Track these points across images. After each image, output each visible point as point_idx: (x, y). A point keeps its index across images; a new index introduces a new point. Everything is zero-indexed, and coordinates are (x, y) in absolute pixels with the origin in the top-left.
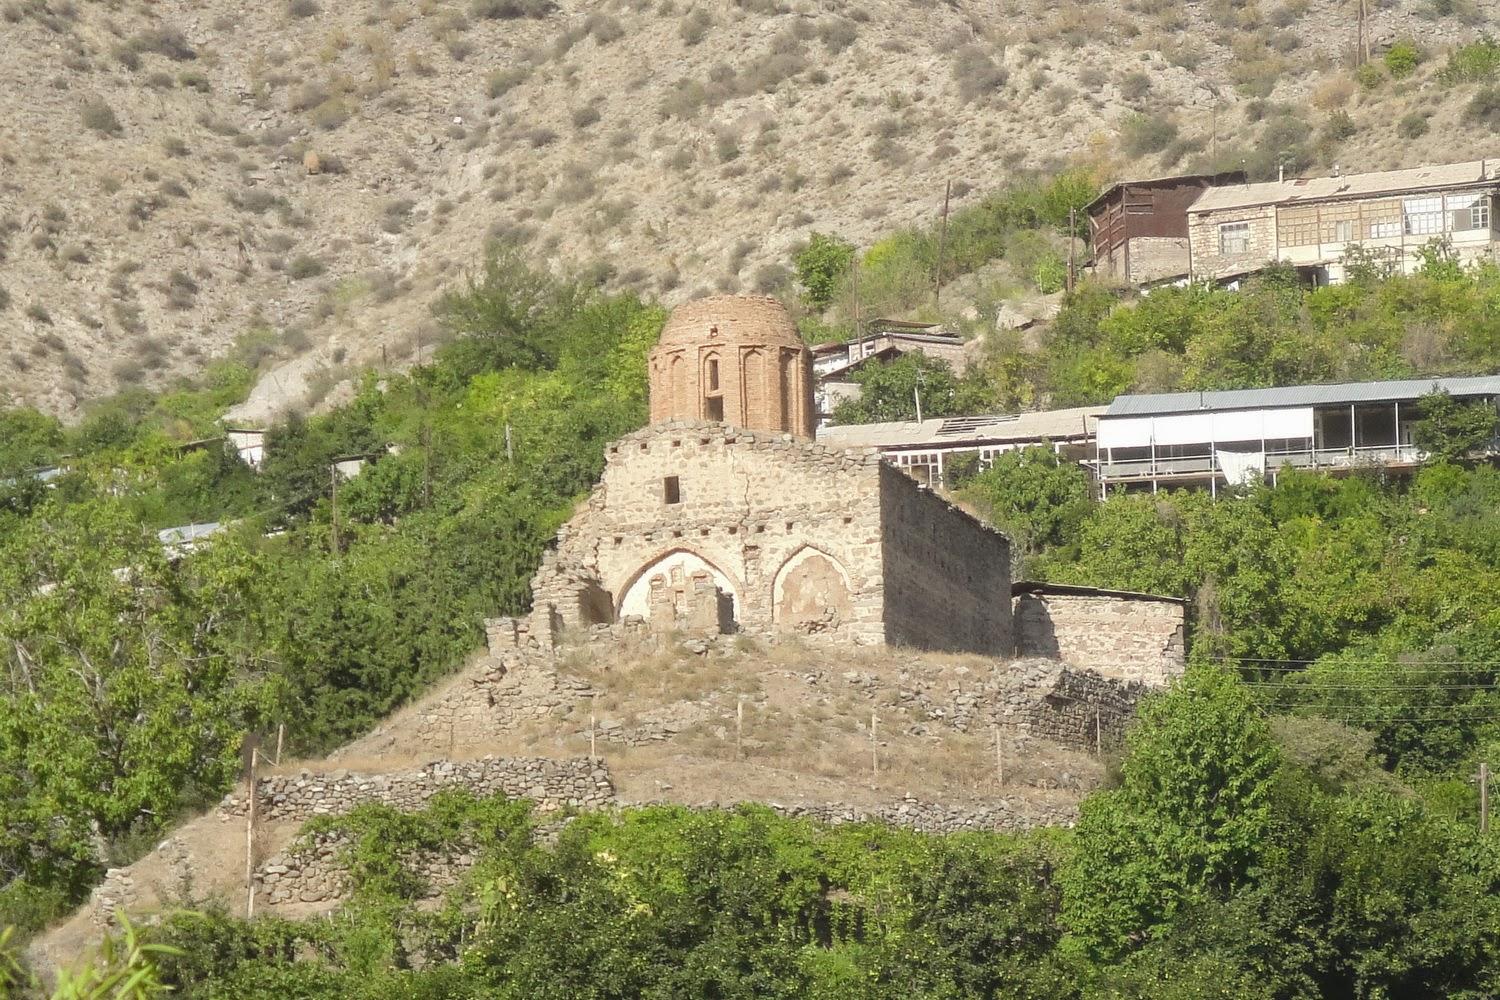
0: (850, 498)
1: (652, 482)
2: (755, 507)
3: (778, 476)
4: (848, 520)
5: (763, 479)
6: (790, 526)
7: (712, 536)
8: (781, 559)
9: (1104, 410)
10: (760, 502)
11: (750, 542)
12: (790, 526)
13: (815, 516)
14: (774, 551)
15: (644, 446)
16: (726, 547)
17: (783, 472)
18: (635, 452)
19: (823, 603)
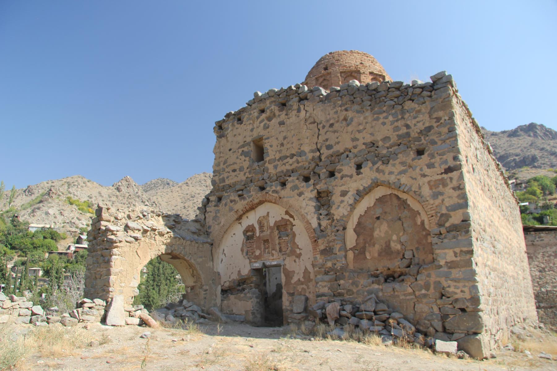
0: (421, 126)
1: (243, 146)
2: (325, 152)
3: (345, 119)
4: (420, 153)
5: (332, 125)
6: (359, 167)
7: (289, 185)
8: (351, 201)
9: (291, 219)
10: (329, 147)
11: (321, 186)
12: (359, 167)
13: (384, 152)
14: (344, 194)
15: (239, 119)
16: (300, 194)
17: (350, 114)
18: (233, 125)
19: (399, 247)
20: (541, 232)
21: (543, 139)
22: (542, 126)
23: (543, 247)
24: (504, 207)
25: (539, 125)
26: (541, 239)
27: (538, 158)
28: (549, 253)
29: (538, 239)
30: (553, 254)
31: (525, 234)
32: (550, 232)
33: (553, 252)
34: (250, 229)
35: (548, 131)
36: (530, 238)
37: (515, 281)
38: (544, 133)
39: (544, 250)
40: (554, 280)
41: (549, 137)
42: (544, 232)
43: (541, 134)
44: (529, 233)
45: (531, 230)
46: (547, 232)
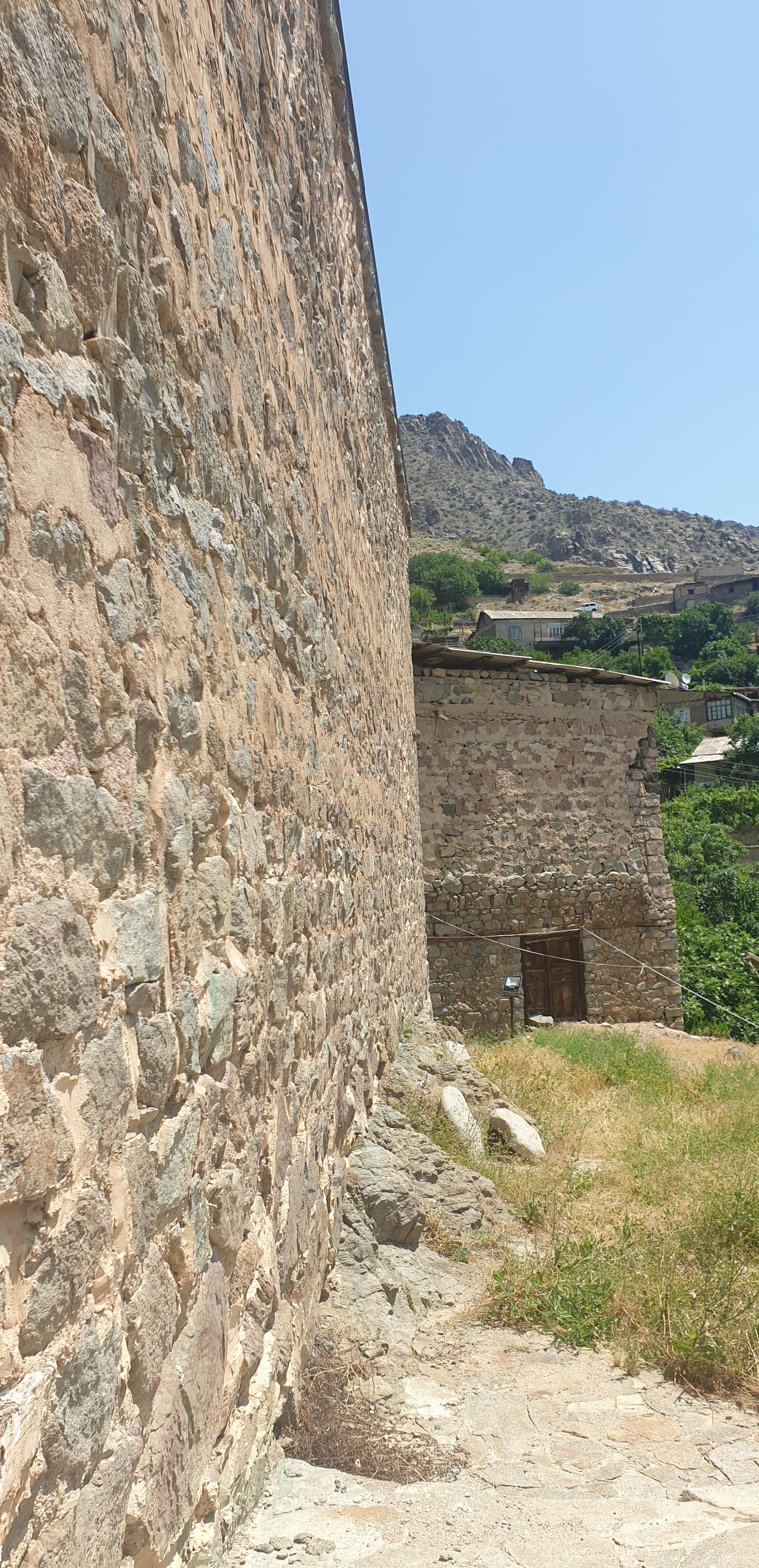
20: (466, 672)
21: (457, 463)
22: (459, 426)
23: (467, 728)
24: (281, 47)
25: (454, 424)
26: (463, 696)
27: (441, 513)
28: (484, 748)
29: (453, 697)
30: (495, 753)
31: (418, 674)
32: (494, 673)
33: (495, 745)
34: (159, 730)
35: (471, 444)
36: (431, 692)
37: (349, 412)
38: (463, 450)
39: (470, 737)
40: (488, 844)
41: (473, 461)
42: (476, 673)
43: (455, 450)
44: (426, 671)
45: (434, 660)
46: (485, 674)
